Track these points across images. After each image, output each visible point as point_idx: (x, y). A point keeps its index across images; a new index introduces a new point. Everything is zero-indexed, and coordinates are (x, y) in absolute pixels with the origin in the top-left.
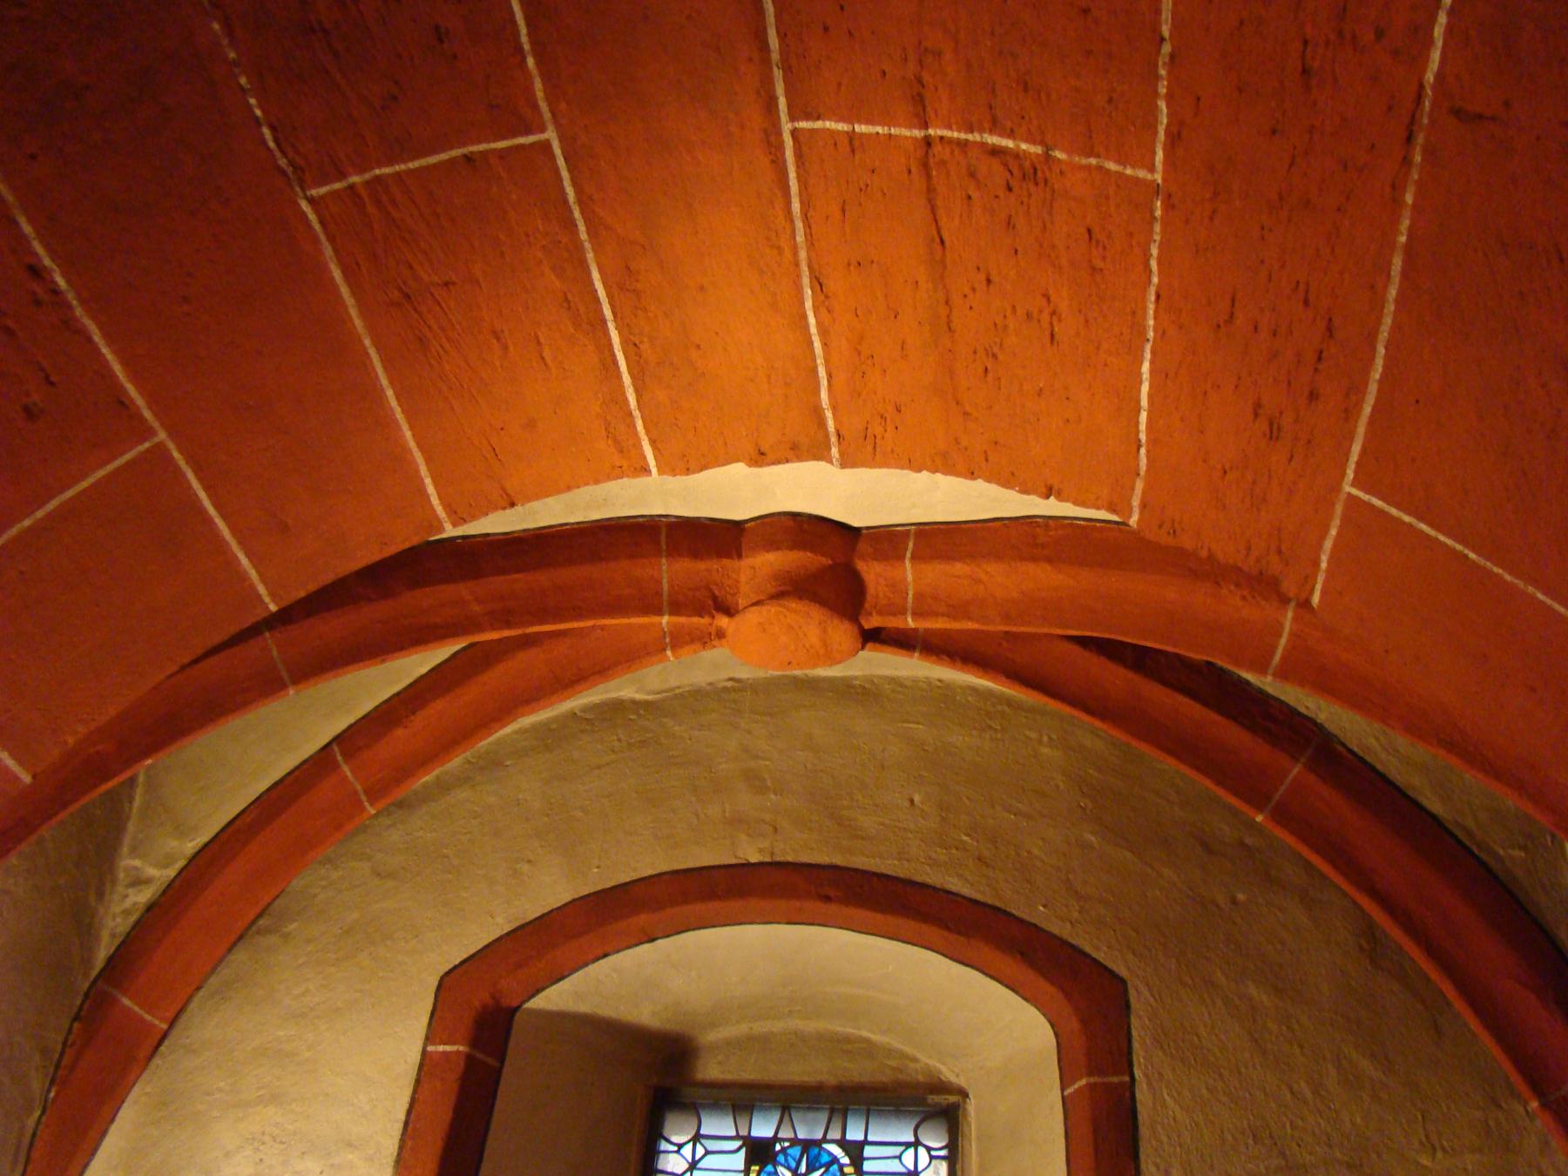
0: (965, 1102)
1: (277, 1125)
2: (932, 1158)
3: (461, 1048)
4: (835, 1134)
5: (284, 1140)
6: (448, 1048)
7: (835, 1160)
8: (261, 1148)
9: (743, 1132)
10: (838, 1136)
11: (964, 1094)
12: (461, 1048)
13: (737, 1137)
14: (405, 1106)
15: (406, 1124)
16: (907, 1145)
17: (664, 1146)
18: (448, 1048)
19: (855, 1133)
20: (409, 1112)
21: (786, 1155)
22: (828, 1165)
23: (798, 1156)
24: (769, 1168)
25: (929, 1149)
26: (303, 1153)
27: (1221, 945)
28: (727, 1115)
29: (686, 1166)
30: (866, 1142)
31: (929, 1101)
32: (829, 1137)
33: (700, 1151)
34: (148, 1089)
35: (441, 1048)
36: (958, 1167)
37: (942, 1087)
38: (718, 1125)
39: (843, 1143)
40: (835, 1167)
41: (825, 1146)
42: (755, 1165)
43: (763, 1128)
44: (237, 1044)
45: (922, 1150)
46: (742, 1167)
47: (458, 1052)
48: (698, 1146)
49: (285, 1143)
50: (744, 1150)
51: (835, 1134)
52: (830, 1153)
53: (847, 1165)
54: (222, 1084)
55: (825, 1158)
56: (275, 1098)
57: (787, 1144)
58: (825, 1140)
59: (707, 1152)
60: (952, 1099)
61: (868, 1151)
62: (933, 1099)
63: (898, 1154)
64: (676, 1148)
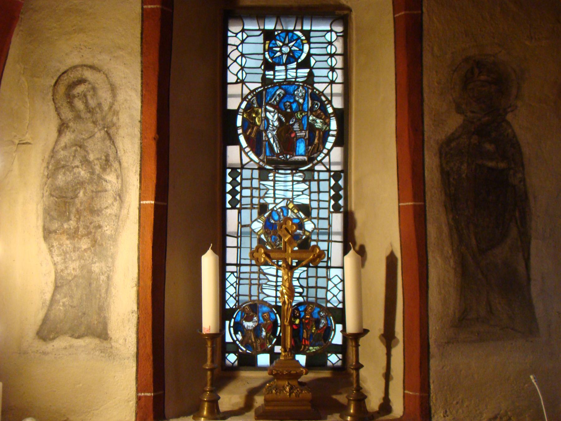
0: (350, 14)
1: (85, 41)
2: (337, 36)
3: (158, 6)
4: (299, 28)
5: (90, 47)
6: (152, 6)
7: (299, 38)
8: (81, 51)
9: (262, 28)
10: (300, 28)
11: (350, 10)
12: (158, 6)
13: (259, 30)
14: (140, 32)
15: (142, 39)
16: (328, 31)
17: (230, 34)
18: (152, 6)
19: (306, 27)
20: (142, 34)
21: (280, 36)
22: (297, 40)
23: (284, 37)
24: (273, 42)
25: (336, 33)
26: (100, 52)
27: (502, 165)
28: (254, 20)
29: (240, 42)
30: (311, 31)
31: (336, 13)
32: (297, 28)
33: (245, 36)
34: (21, 28)
35: (149, 7)
36: (348, 40)
37: (342, 7)
38: (251, 25)
39: (302, 31)
40: (299, 41)
41: (295, 32)
42: (268, 41)
43: (270, 26)
44: (56, 7)
45: (333, 33)
46: (262, 42)
47: (157, 8)
48: (244, 33)
49: (90, 49)
50: (262, 35)
51: (299, 28)
52: (297, 35)
53: (304, 40)
54: (55, 25)
55: (295, 37)
56: (82, 30)
57: (279, 32)
58: (294, 30)
59: (248, 36)
60: (346, 12)
61: (312, 34)
62: (338, 12)
63: (324, 35)
64: (235, 35)
